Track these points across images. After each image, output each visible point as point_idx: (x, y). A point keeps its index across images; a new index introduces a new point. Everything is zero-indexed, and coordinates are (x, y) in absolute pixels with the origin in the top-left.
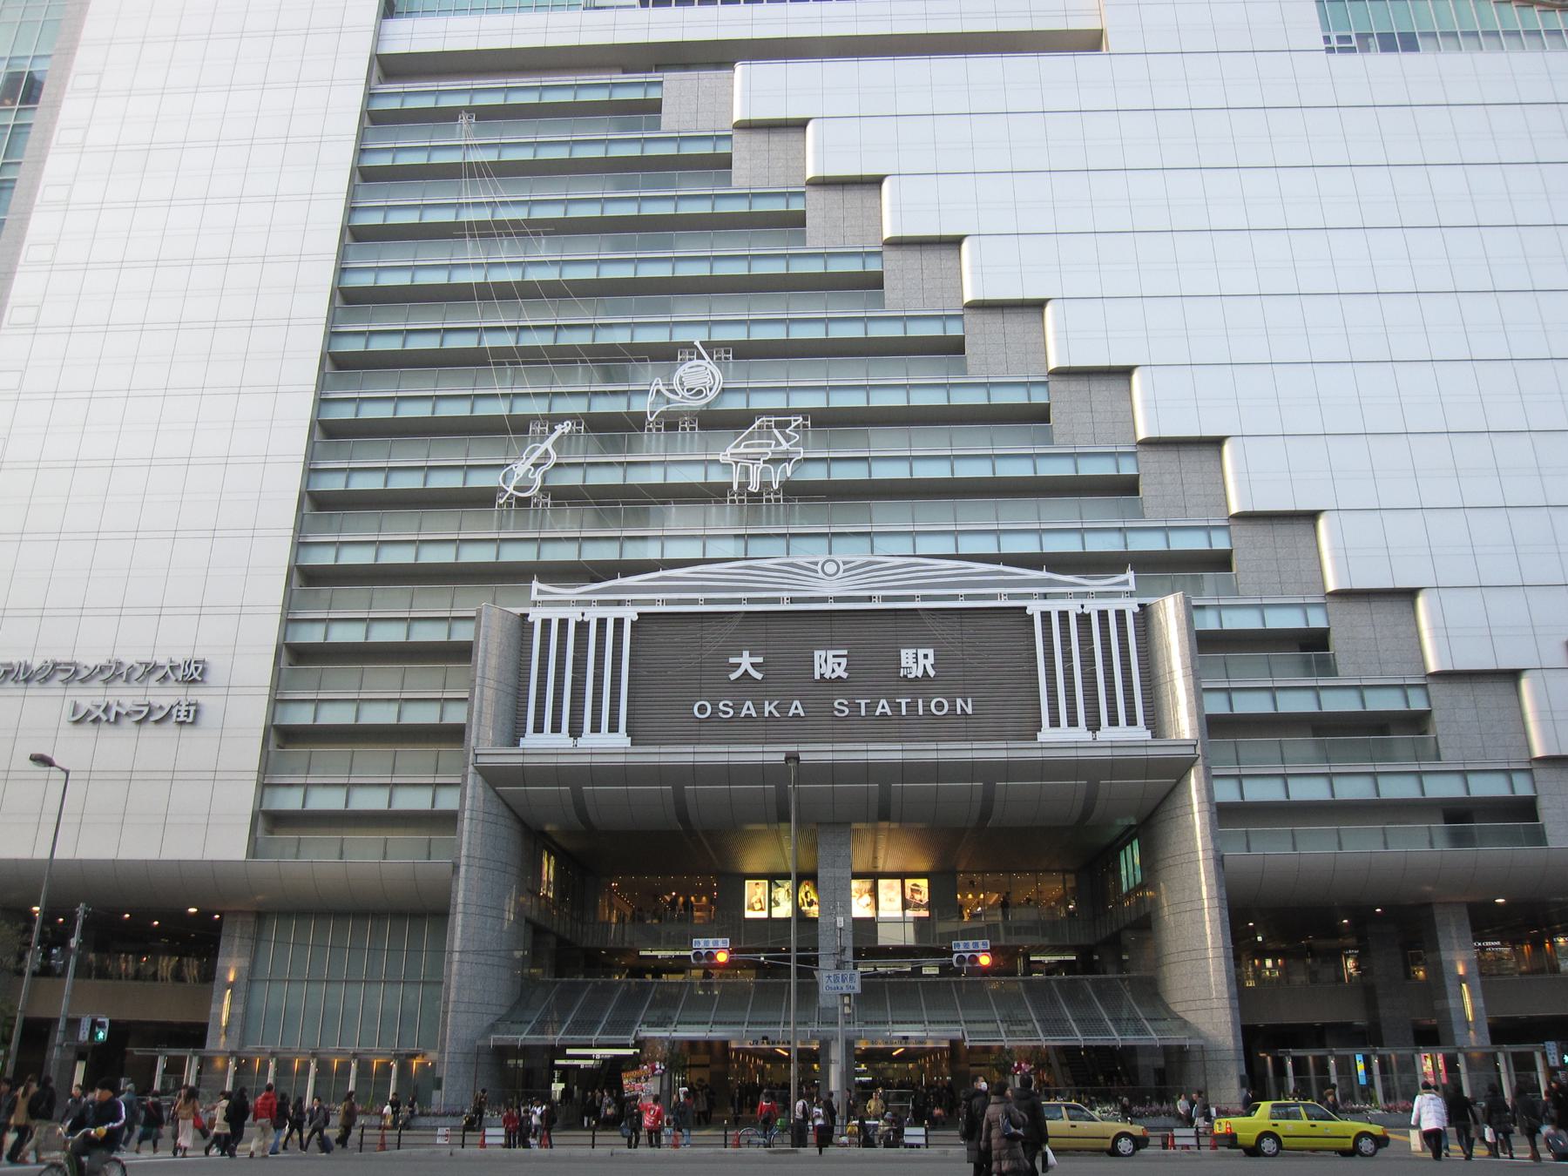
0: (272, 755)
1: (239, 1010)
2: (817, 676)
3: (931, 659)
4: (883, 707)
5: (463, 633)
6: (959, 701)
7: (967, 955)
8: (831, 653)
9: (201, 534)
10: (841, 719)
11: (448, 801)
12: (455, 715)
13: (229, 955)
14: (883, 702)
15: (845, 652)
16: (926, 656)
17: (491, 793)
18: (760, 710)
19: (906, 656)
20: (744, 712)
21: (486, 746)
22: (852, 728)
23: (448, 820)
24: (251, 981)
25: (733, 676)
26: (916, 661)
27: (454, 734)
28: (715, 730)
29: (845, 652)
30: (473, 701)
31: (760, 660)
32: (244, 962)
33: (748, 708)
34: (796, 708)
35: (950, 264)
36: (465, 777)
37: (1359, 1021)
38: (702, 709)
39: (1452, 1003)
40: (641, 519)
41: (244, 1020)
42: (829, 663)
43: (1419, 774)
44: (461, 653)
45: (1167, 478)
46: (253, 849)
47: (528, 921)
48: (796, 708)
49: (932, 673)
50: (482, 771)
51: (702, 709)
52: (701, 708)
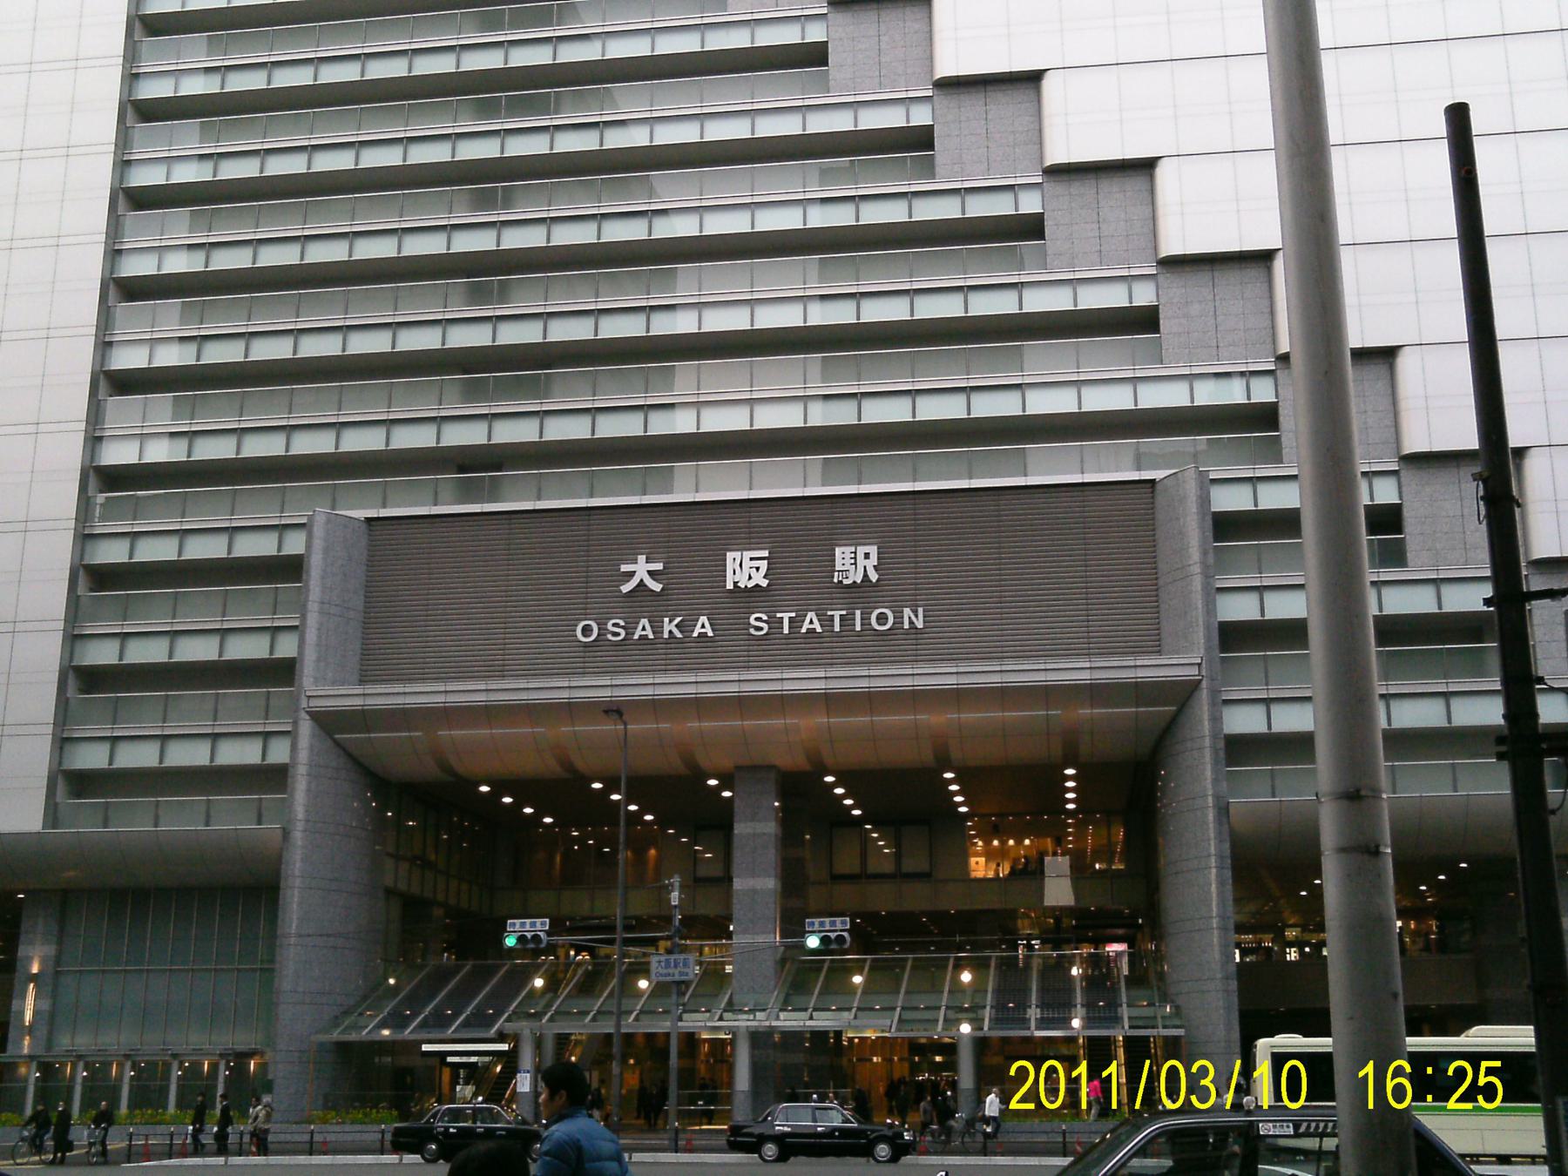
0: (72, 702)
1: (46, 1005)
2: (730, 586)
3: (874, 560)
4: (811, 622)
5: (295, 545)
6: (907, 612)
7: (833, 935)
8: (748, 554)
9: (21, 429)
10: (616, 644)
11: (279, 753)
12: (286, 648)
13: (31, 943)
14: (811, 615)
15: (765, 554)
16: (867, 556)
17: (329, 743)
18: (657, 630)
19: (842, 555)
20: (638, 633)
21: (325, 688)
22: (773, 650)
23: (273, 777)
24: (57, 974)
25: (626, 588)
26: (855, 562)
27: (281, 672)
28: (603, 655)
29: (765, 554)
30: (309, 634)
31: (659, 566)
32: (51, 950)
33: (644, 628)
34: (703, 626)
35: (917, 26)
36: (295, 723)
37: (1469, 1000)
38: (587, 631)
39: (15, 1004)
40: (538, 389)
41: (50, 1019)
42: (745, 568)
43: (1446, 696)
44: (289, 569)
45: (1195, 309)
46: (52, 814)
47: (389, 892)
48: (703, 626)
49: (874, 577)
50: (318, 717)
51: (587, 631)
52: (584, 630)
